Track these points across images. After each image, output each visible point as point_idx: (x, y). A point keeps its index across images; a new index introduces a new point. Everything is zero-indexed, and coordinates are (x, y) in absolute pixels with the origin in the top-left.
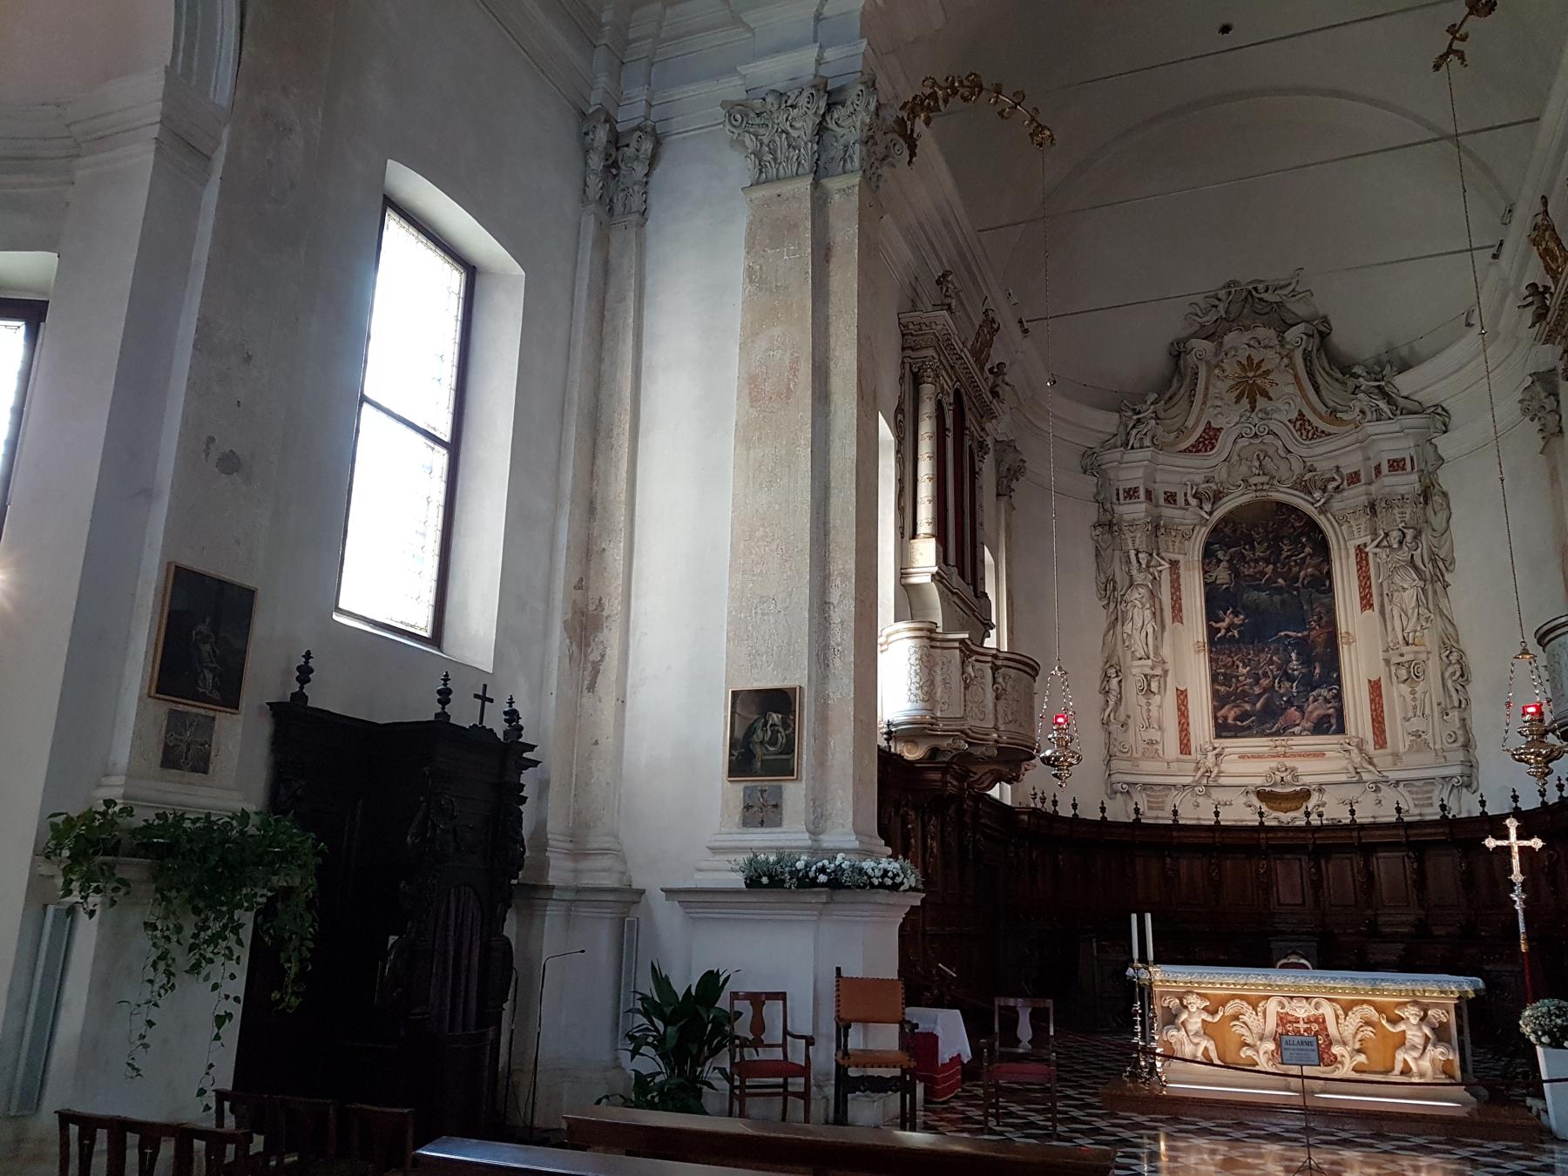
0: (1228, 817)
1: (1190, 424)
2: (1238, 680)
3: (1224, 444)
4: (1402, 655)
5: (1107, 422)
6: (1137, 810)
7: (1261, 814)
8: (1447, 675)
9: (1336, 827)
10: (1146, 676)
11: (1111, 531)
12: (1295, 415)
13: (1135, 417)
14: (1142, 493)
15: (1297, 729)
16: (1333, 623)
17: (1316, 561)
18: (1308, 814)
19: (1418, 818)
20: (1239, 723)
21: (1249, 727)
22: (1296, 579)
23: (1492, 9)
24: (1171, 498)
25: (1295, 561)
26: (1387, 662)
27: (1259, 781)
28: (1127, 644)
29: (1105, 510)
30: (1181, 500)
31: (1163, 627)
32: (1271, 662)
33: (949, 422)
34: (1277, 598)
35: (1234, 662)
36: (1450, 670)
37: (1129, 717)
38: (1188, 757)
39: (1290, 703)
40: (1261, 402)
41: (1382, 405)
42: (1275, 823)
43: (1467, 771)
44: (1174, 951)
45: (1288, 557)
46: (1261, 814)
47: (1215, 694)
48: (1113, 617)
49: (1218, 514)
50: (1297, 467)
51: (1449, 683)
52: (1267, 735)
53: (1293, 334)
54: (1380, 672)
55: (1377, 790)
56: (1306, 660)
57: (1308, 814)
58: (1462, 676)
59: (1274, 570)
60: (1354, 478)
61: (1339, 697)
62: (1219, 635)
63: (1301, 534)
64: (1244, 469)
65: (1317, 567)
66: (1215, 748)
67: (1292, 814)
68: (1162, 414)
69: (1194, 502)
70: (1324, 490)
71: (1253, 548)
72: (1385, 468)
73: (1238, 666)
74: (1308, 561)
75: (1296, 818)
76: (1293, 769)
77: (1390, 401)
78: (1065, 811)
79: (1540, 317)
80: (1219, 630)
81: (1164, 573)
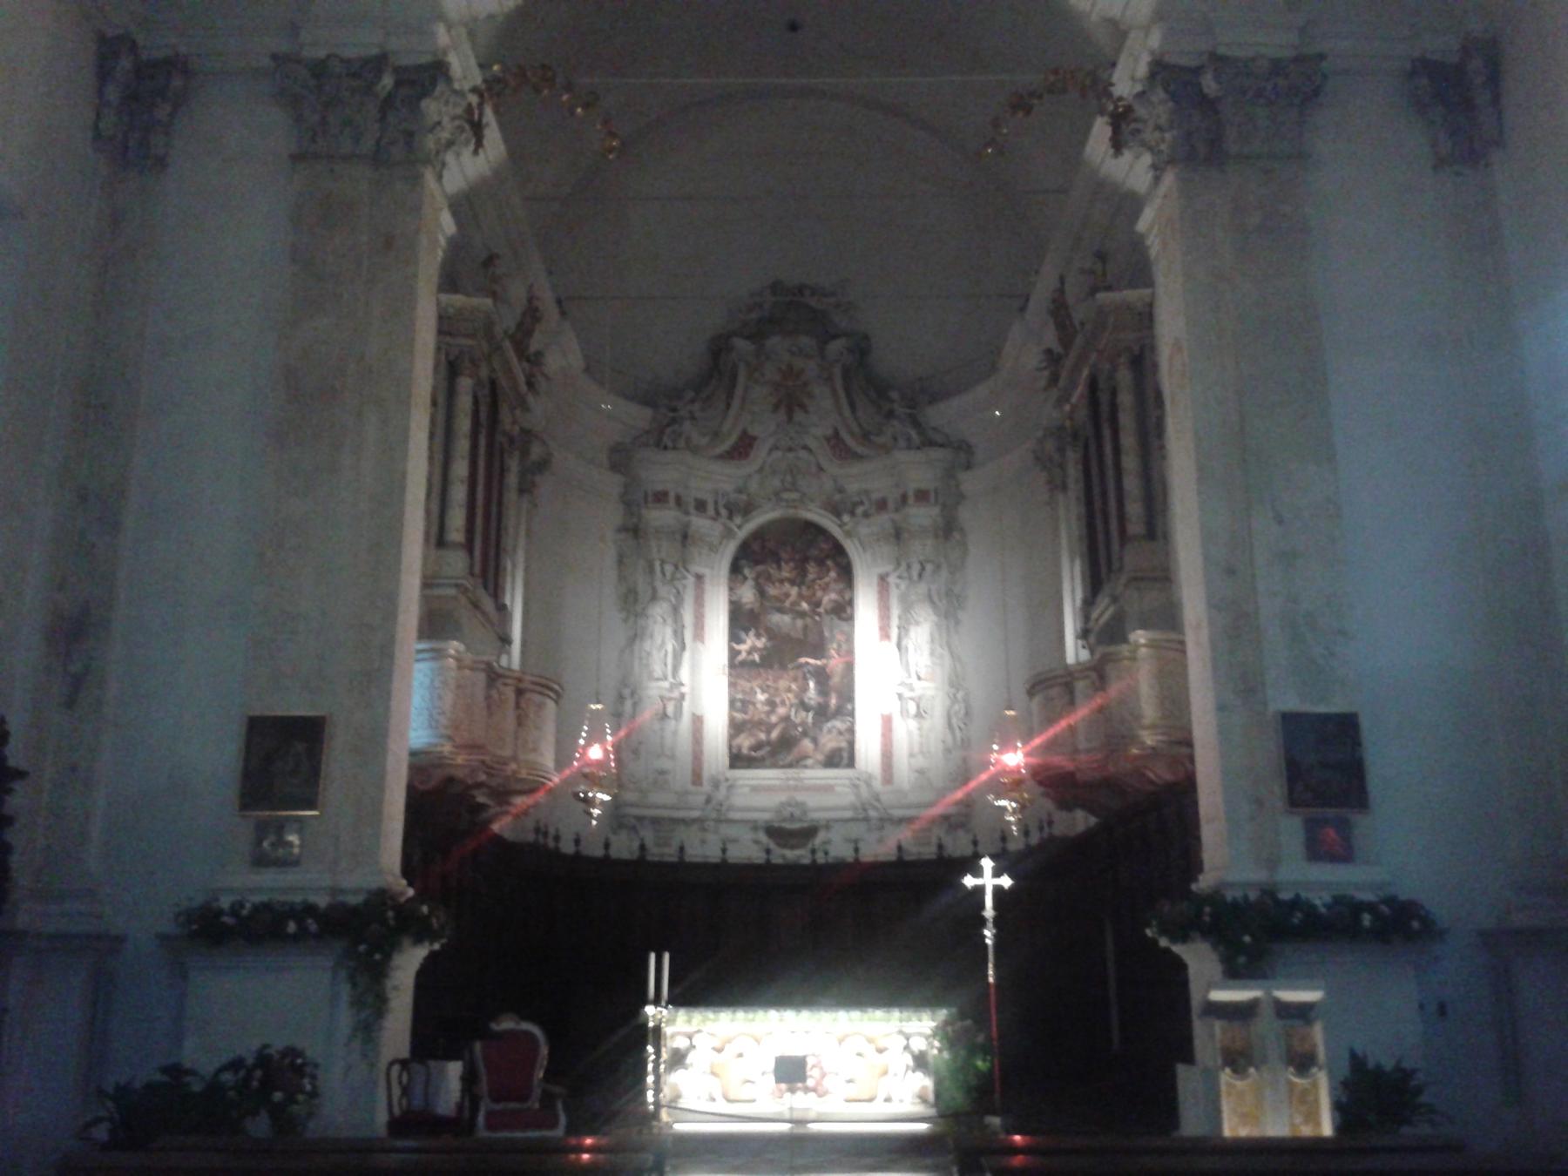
0: (738, 854)
3: (760, 455)
5: (640, 416)
7: (768, 851)
9: (839, 866)
10: (662, 698)
12: (830, 432)
14: (672, 495)
15: (809, 762)
16: (851, 652)
18: (813, 852)
19: (784, 1128)
20: (753, 753)
22: (818, 604)
23: (969, 446)
24: (701, 506)
26: (900, 696)
27: (766, 816)
30: (711, 510)
31: (683, 647)
32: (789, 690)
33: (483, 415)
34: (800, 623)
38: (699, 788)
39: (805, 734)
40: (799, 416)
41: (913, 434)
44: (688, 995)
46: (768, 851)
50: (828, 485)
51: (954, 721)
52: (783, 767)
53: (836, 346)
54: (894, 708)
55: (881, 828)
56: (823, 690)
57: (813, 852)
58: (967, 714)
60: (882, 505)
61: (851, 731)
63: (828, 557)
65: (840, 593)
66: (727, 780)
67: (798, 852)
69: (724, 512)
70: (852, 513)
71: (779, 568)
74: (833, 586)
75: (800, 855)
78: (568, 847)
79: (1054, 380)
80: (739, 652)
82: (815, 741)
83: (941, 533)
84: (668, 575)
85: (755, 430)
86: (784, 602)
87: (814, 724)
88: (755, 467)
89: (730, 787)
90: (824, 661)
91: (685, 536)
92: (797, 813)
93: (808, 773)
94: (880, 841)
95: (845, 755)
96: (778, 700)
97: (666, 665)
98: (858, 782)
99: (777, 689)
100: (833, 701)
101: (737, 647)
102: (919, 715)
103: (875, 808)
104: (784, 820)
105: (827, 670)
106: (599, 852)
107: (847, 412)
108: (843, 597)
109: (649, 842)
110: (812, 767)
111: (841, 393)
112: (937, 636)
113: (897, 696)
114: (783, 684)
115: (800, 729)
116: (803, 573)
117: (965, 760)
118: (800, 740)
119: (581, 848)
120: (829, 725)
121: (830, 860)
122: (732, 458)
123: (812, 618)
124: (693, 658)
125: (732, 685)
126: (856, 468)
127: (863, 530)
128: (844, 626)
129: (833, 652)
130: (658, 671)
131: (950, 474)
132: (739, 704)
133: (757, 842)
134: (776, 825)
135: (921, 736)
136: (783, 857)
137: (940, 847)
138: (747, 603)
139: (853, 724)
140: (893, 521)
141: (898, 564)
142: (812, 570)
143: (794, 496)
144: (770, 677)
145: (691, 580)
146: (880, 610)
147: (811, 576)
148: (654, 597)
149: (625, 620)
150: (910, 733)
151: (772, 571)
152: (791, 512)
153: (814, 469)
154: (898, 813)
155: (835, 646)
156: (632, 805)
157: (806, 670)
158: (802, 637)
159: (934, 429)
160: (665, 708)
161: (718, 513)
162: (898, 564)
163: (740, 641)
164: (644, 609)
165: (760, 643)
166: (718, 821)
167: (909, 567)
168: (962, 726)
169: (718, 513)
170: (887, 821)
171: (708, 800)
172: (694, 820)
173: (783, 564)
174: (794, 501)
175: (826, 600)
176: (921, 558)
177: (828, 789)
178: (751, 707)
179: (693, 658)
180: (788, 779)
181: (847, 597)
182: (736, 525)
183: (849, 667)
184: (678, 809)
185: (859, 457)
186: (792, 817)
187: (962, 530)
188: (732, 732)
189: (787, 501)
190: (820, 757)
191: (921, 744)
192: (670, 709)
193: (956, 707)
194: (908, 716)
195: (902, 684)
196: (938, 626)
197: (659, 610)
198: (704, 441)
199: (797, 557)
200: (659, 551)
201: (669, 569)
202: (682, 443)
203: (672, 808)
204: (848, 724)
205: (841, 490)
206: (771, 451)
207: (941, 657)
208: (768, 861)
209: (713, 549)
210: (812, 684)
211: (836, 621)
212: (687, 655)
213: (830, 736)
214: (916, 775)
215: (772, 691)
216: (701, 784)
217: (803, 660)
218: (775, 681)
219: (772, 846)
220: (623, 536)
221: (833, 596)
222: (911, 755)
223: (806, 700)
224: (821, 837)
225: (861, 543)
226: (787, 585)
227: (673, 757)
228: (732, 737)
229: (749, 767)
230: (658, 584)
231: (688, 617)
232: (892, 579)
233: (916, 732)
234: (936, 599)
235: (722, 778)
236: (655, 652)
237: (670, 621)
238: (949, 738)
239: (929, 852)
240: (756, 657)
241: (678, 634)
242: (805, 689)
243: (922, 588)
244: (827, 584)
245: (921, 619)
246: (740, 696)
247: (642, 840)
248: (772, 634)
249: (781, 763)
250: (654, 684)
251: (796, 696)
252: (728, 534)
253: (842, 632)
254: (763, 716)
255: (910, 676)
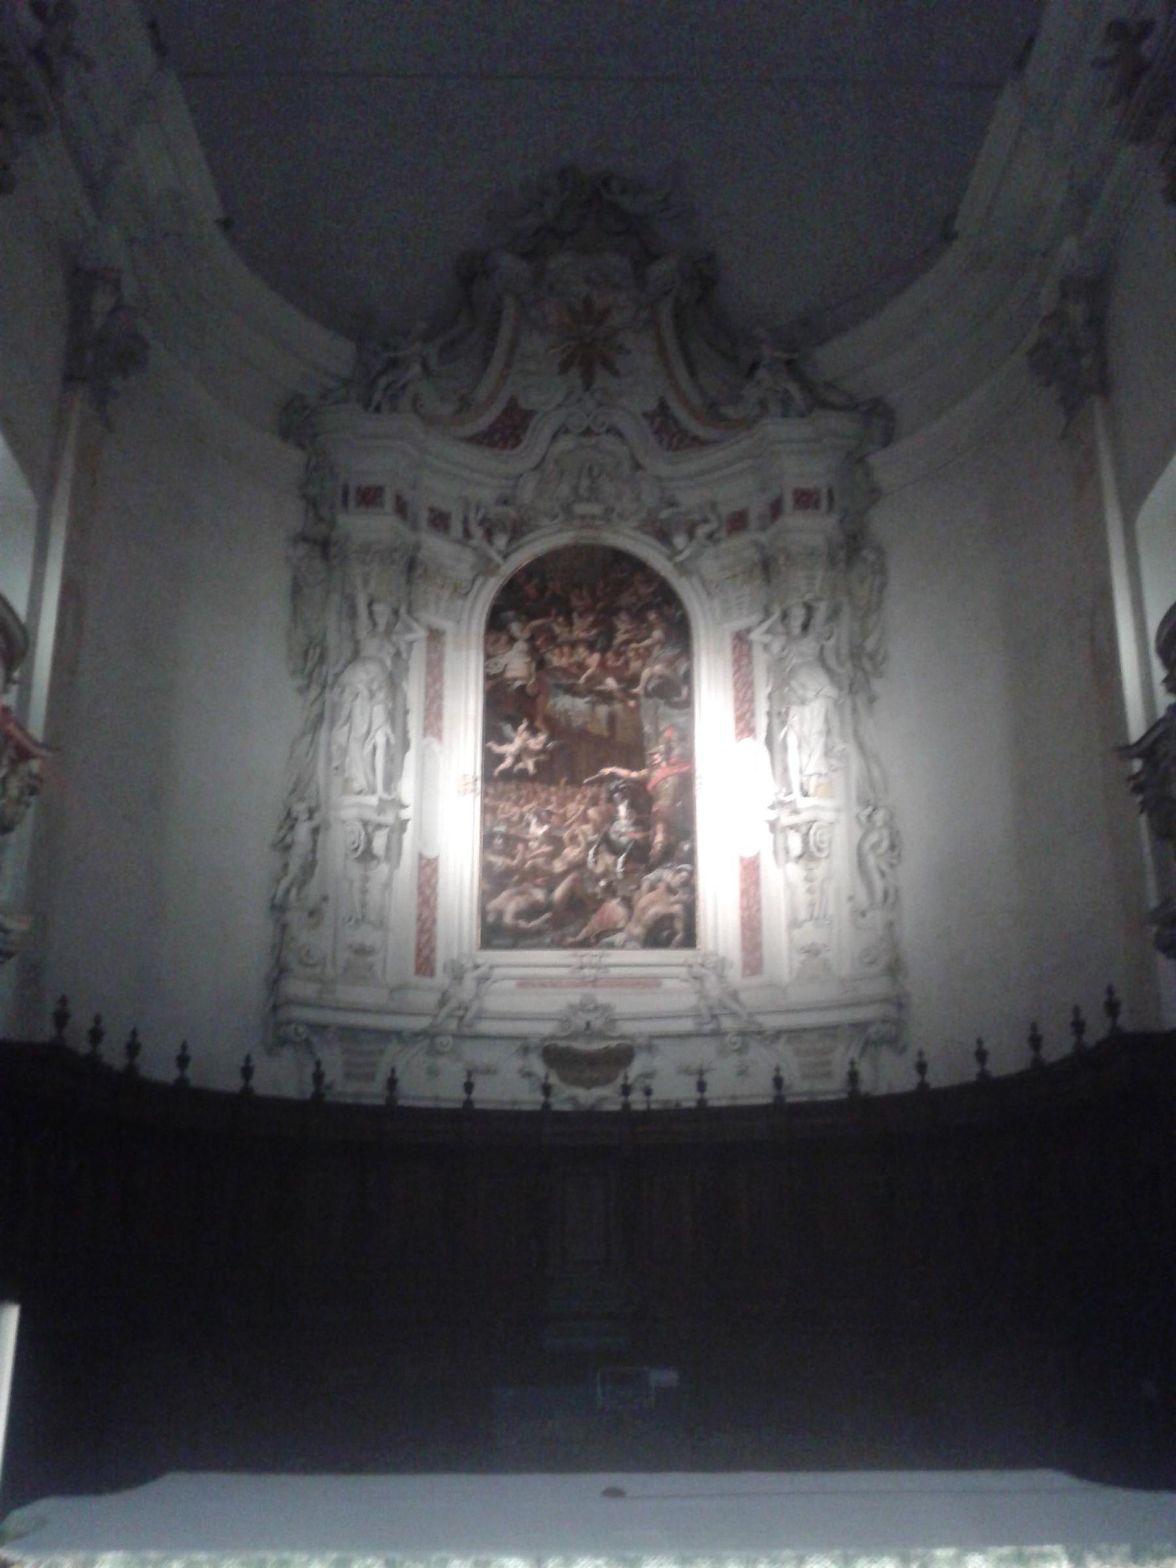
0: (488, 1094)
1: (482, 392)
2: (527, 848)
4: (796, 812)
6: (318, 1077)
7: (547, 1089)
8: (867, 846)
9: (672, 1116)
10: (365, 824)
11: (325, 555)
12: (652, 405)
13: (385, 355)
14: (389, 498)
15: (619, 938)
16: (688, 758)
17: (669, 652)
18: (626, 1090)
20: (522, 924)
21: (538, 932)
22: (634, 680)
24: (440, 521)
25: (637, 650)
26: (773, 826)
27: (547, 1028)
28: (335, 763)
29: (320, 519)
30: (457, 528)
31: (405, 745)
32: (584, 819)
34: (603, 710)
35: (522, 817)
36: (874, 838)
37: (325, 899)
38: (426, 981)
39: (610, 891)
40: (602, 378)
41: (793, 389)
42: (567, 1107)
43: (891, 1011)
45: (627, 643)
46: (547, 1089)
47: (487, 870)
48: (316, 709)
49: (522, 557)
51: (871, 861)
53: (662, 270)
54: (761, 844)
57: (626, 1090)
58: (892, 847)
59: (602, 664)
60: (738, 522)
61: (689, 885)
62: (502, 766)
63: (649, 606)
64: (565, 490)
65: (671, 663)
66: (477, 967)
67: (599, 1092)
68: (433, 362)
69: (478, 533)
70: (691, 535)
71: (570, 623)
72: (788, 502)
73: (528, 825)
74: (656, 651)
76: (606, 1008)
77: (807, 386)
80: (501, 758)
81: (416, 646)
82: (628, 902)
83: (841, 555)
84: (382, 622)
85: (532, 400)
86: (578, 678)
87: (625, 873)
88: (534, 459)
89: (482, 980)
90: (644, 772)
91: (411, 565)
92: (597, 1024)
93: (615, 956)
94: (743, 1072)
95: (679, 925)
96: (566, 835)
97: (374, 770)
98: (703, 971)
99: (564, 817)
100: (659, 839)
101: (498, 749)
102: (806, 855)
103: (733, 1014)
104: (574, 1036)
105: (650, 786)
106: (233, 1083)
107: (681, 373)
108: (675, 670)
109: (334, 1072)
110: (623, 946)
111: (672, 346)
112: (835, 723)
113: (767, 826)
114: (574, 809)
115: (602, 883)
116: (609, 633)
117: (890, 925)
118: (601, 902)
119: (190, 1072)
120: (652, 876)
121: (654, 1106)
122: (492, 444)
123: (623, 701)
124: (422, 759)
125: (485, 809)
126: (693, 462)
127: (709, 565)
128: (680, 719)
129: (658, 758)
130: (360, 782)
131: (856, 460)
132: (498, 842)
133: (528, 1075)
134: (562, 1044)
135: (810, 891)
136: (573, 1099)
137: (853, 1077)
138: (515, 679)
139: (692, 874)
140: (756, 544)
141: (767, 613)
142: (623, 627)
143: (595, 509)
144: (554, 799)
145: (420, 633)
146: (737, 690)
147: (620, 637)
148: (356, 656)
149: (303, 690)
150: (789, 885)
151: (557, 630)
152: (587, 536)
153: (626, 467)
154: (771, 1022)
155: (662, 747)
156: (305, 1004)
157: (612, 786)
158: (606, 734)
159: (829, 385)
160: (369, 841)
161: (467, 534)
162: (767, 613)
163: (503, 740)
164: (337, 676)
165: (537, 743)
166: (459, 1036)
167: (785, 616)
168: (885, 867)
169: (467, 534)
170: (752, 1034)
171: (443, 1002)
172: (418, 1035)
173: (575, 615)
174: (594, 517)
175: (646, 673)
176: (808, 597)
177: (651, 983)
178: (520, 847)
179: (422, 759)
180: (582, 967)
181: (682, 669)
182: (499, 552)
183: (686, 785)
184: (395, 1013)
185: (699, 443)
186: (588, 1031)
187: (879, 550)
188: (487, 887)
189: (583, 517)
190: (638, 930)
191: (812, 905)
192: (379, 843)
193: (874, 838)
194: (787, 860)
195: (780, 804)
196: (838, 705)
197: (361, 677)
198: (446, 410)
199: (600, 605)
200: (366, 583)
201: (382, 611)
202: (405, 403)
203: (380, 1011)
204: (684, 874)
205: (672, 504)
206: (555, 437)
207: (843, 756)
208: (546, 1106)
209: (461, 591)
210: (622, 810)
211: (663, 709)
212: (411, 758)
213: (652, 895)
214: (804, 957)
215: (554, 819)
216: (432, 973)
217: (607, 771)
218: (562, 804)
219: (554, 1079)
220: (302, 549)
221: (658, 668)
222: (794, 924)
223: (613, 836)
224: (636, 1069)
225: (704, 582)
226: (582, 651)
227: (381, 924)
228: (486, 896)
229: (514, 946)
230: (363, 632)
231: (414, 692)
232: (756, 636)
233: (802, 887)
234: (832, 662)
235: (469, 965)
236: (354, 748)
237: (381, 696)
238: (862, 899)
239: (832, 1087)
240: (530, 765)
241: (397, 717)
242: (611, 818)
243: (809, 646)
244: (649, 650)
245: (810, 694)
246: (502, 829)
247: (318, 1064)
248: (555, 727)
249: (570, 940)
250: (351, 799)
251: (596, 830)
252: (486, 568)
253: (673, 726)
254: (540, 861)
255: (790, 793)
